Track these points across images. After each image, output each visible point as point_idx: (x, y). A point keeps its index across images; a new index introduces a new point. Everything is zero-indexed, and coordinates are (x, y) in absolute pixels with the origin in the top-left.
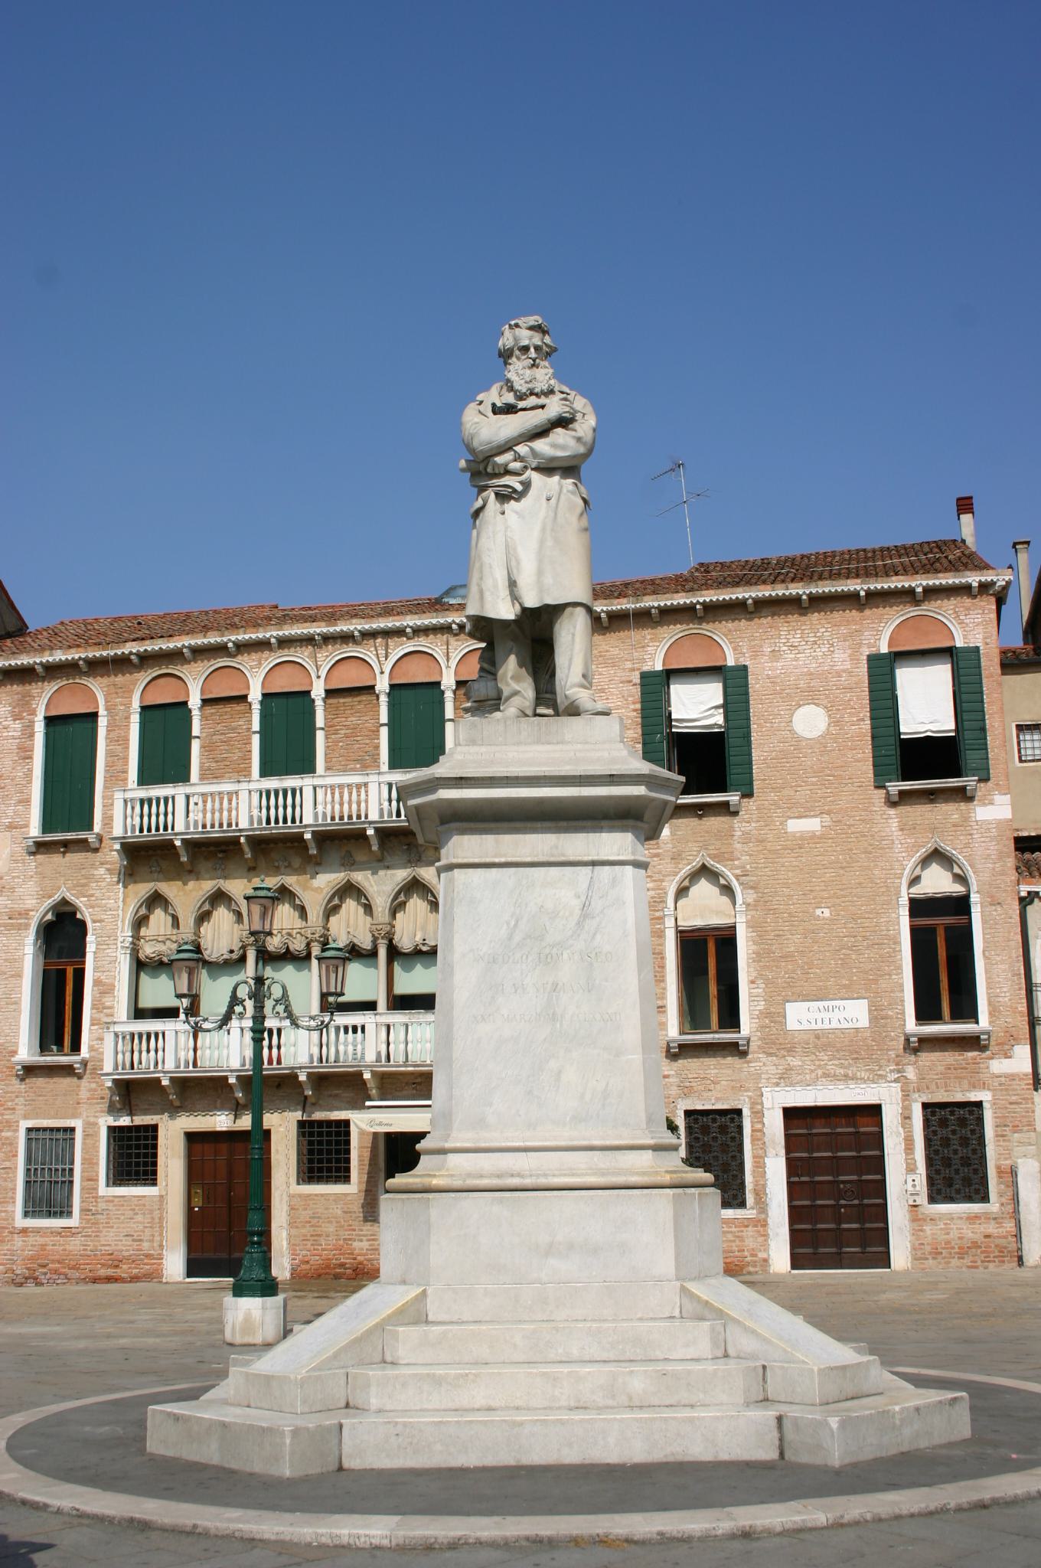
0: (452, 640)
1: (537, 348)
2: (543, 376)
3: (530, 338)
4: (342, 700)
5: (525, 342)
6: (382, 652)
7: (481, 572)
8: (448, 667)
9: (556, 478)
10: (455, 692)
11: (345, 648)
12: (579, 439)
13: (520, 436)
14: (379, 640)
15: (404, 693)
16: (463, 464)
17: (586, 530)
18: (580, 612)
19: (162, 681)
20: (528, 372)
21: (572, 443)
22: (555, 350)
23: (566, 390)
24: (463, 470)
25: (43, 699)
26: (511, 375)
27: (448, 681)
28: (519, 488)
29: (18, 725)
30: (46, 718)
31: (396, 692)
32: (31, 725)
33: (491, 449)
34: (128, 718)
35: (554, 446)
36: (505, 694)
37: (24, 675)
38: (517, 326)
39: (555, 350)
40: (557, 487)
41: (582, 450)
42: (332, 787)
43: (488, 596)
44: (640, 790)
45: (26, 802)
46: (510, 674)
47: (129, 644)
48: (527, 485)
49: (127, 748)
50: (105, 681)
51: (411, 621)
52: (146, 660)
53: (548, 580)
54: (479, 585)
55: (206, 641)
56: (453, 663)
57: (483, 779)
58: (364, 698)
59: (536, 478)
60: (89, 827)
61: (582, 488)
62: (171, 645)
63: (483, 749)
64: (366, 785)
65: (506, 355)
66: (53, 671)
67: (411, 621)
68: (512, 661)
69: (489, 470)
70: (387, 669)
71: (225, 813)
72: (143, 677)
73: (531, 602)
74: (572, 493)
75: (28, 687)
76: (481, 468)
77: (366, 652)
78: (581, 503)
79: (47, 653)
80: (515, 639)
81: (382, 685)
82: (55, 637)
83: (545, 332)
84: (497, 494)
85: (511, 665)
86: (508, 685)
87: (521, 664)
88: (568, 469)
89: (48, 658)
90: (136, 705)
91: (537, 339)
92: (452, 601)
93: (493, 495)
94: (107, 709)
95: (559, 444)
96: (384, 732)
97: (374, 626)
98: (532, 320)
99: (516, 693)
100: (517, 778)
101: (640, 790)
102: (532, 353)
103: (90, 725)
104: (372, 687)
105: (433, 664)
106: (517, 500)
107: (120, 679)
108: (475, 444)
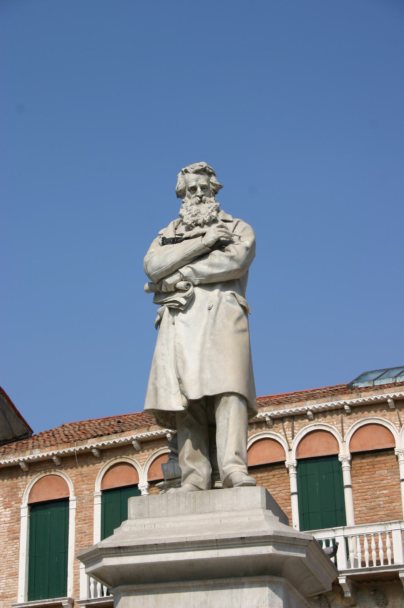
0: (346, 419)
1: (203, 188)
2: (206, 210)
3: (197, 180)
4: (259, 475)
5: (193, 184)
6: (289, 433)
7: (156, 373)
8: (343, 441)
9: (217, 291)
10: (350, 462)
11: (259, 431)
12: (232, 258)
13: (183, 260)
14: (286, 423)
15: (309, 465)
16: (146, 286)
17: (244, 331)
18: (233, 400)
19: (118, 468)
20: (195, 207)
21: (226, 261)
22: (220, 187)
23: (229, 217)
24: (147, 291)
25: (27, 489)
26: (183, 212)
27: (344, 454)
28: (184, 302)
29: (8, 512)
30: (29, 505)
31: (303, 465)
32: (18, 511)
33: (162, 273)
34: (92, 501)
35: (211, 265)
36: (184, 472)
37: (12, 471)
38: (186, 171)
39: (220, 187)
40: (216, 299)
41: (235, 266)
42: (361, 536)
43: (161, 392)
44: (268, 550)
45: (15, 575)
46: (186, 456)
47: (89, 441)
48: (191, 299)
49: (92, 525)
50: (74, 471)
51: (310, 405)
52: (105, 452)
53: (207, 375)
54: (154, 384)
55: (149, 434)
56: (348, 438)
57: (137, 547)
58: (276, 472)
59: (198, 291)
60: (64, 593)
61: (240, 298)
62: (123, 439)
63: (147, 521)
64: (390, 533)
65: (181, 195)
66: (34, 466)
67: (310, 405)
68: (188, 443)
69: (163, 289)
70: (294, 447)
71: (381, 553)
72: (103, 467)
73: (195, 394)
74: (231, 302)
75: (15, 481)
76: (158, 289)
77: (277, 433)
78: (240, 309)
79: (28, 452)
80: (190, 426)
81: (291, 460)
82: (51, 437)
83: (210, 174)
84: (170, 309)
85: (187, 447)
86: (185, 465)
87: (196, 447)
88: (233, 282)
89: (29, 456)
90: (98, 489)
91: (203, 180)
92: (361, 385)
93: (167, 310)
94: (76, 495)
95: (218, 263)
96: (295, 499)
97: (281, 412)
98: (197, 166)
99: (192, 471)
100: (165, 545)
101: (268, 550)
102: (199, 192)
103: (63, 509)
104: (283, 463)
105: (331, 440)
106: (184, 312)
107: (85, 469)
108: (149, 270)
